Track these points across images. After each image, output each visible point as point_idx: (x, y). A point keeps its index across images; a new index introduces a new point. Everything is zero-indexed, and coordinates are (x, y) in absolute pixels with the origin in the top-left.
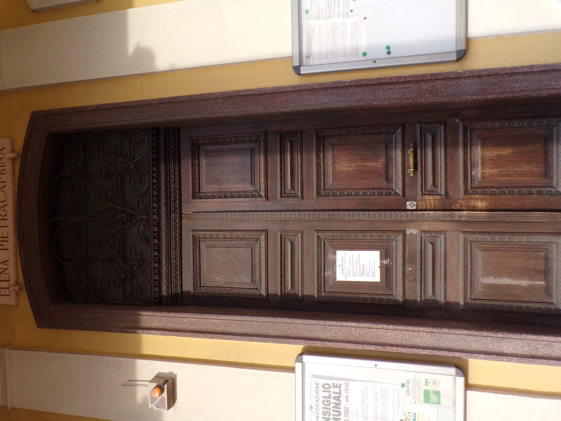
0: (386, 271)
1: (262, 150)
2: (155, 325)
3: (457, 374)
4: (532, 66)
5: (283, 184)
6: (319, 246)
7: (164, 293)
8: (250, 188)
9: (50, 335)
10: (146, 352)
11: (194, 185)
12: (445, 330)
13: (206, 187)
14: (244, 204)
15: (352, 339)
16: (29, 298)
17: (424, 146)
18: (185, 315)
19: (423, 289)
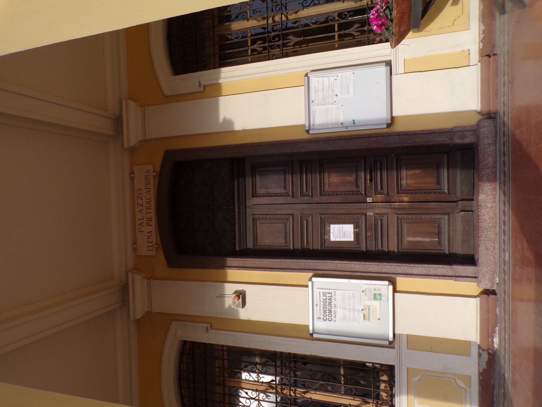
0: (357, 235)
1: (290, 171)
2: (234, 265)
3: (389, 285)
4: (423, 131)
5: (302, 189)
6: (321, 223)
7: (237, 249)
8: (283, 191)
9: (175, 272)
10: (229, 280)
11: (253, 190)
12: (385, 264)
13: (260, 191)
14: (281, 200)
15: (337, 269)
16: (164, 252)
17: (376, 170)
18: (250, 259)
19: (376, 244)
